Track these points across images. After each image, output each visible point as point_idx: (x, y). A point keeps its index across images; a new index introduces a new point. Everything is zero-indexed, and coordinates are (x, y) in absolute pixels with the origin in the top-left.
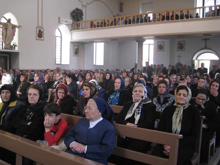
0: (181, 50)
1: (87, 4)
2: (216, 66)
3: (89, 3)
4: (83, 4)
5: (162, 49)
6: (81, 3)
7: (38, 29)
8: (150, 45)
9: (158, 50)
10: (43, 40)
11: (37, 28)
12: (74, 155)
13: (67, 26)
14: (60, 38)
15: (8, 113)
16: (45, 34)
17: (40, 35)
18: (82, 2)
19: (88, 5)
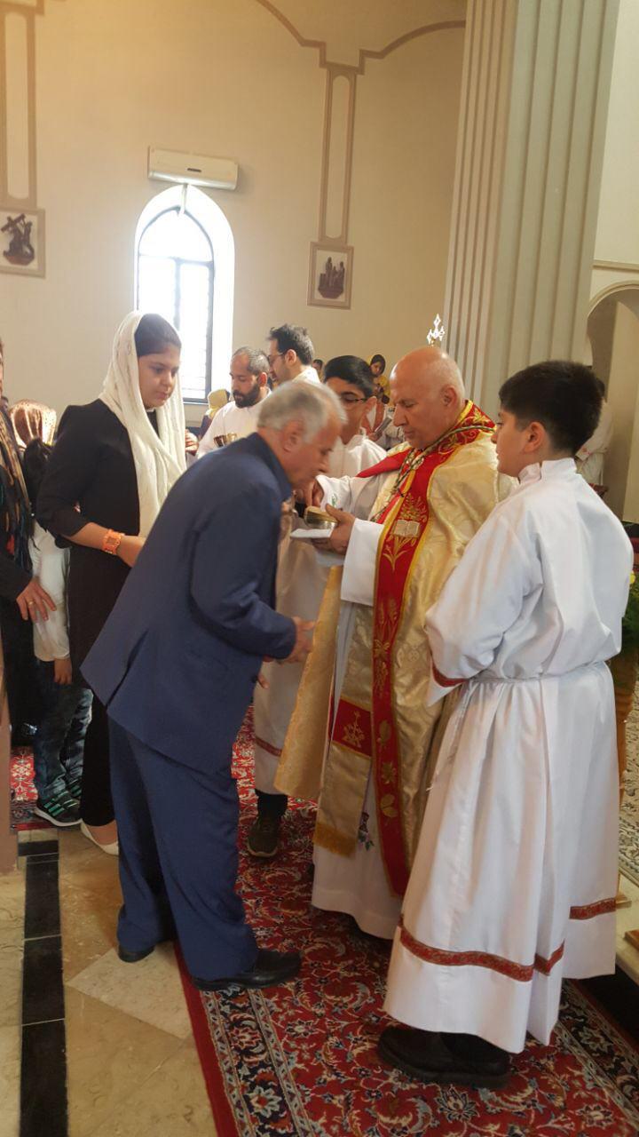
0: (317, 284)
1: (365, 54)
2: (239, 350)
3: (378, 49)
4: (329, 59)
5: (336, 296)
6: (316, 52)
7: (322, 257)
8: (183, 266)
9: (311, 296)
10: (41, 274)
11: (315, 247)
12: (190, 1030)
13: (204, 192)
14: (206, 271)
15: (79, 789)
16: (54, 243)
17: (21, 249)
18: (320, 45)
19: (369, 61)
